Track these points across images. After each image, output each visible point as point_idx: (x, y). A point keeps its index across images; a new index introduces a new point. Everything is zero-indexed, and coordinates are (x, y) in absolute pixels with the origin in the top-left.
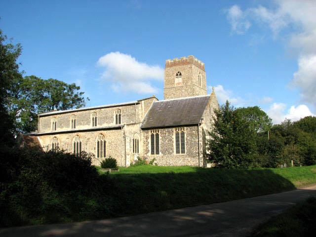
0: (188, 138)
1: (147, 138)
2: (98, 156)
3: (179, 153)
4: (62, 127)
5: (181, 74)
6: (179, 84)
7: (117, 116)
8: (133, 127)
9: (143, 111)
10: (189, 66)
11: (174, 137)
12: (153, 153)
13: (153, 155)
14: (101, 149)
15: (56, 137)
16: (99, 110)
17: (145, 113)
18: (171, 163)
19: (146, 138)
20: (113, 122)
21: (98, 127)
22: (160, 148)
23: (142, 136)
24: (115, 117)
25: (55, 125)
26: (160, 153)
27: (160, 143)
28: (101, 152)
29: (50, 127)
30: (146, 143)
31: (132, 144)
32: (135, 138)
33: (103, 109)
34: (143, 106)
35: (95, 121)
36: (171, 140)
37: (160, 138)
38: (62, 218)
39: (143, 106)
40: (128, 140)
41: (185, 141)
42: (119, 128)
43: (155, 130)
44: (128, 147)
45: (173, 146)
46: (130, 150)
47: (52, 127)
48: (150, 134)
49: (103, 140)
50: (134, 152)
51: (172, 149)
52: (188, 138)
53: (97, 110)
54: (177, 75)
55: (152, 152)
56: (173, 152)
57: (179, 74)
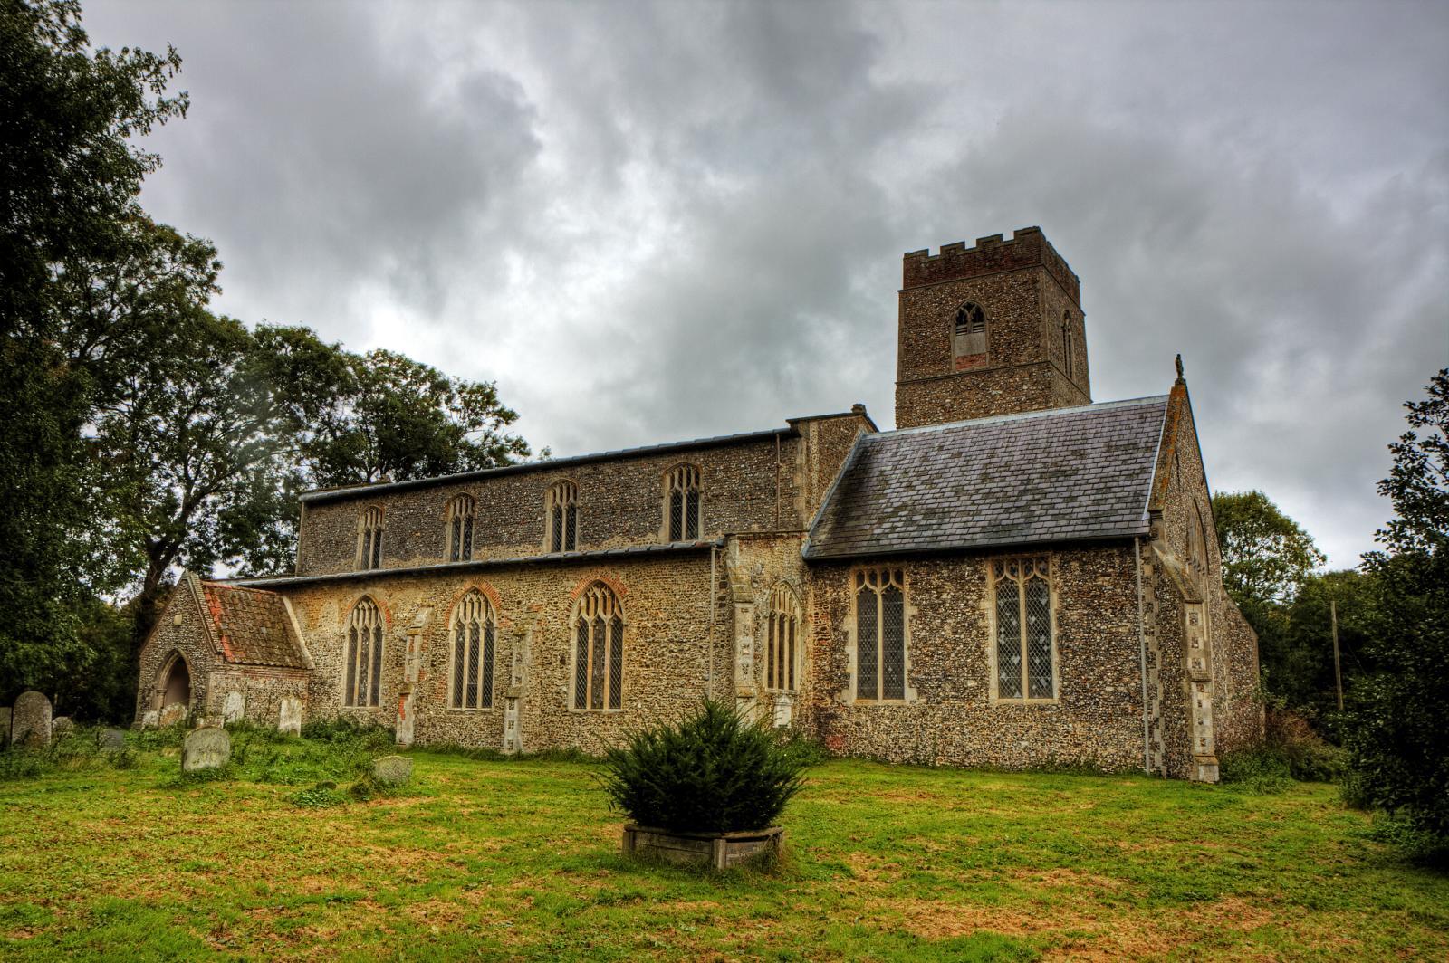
0: (1072, 615)
1: (837, 613)
2: (581, 702)
3: (874, 695)
4: (409, 555)
5: (979, 317)
6: (971, 359)
7: (676, 499)
8: (766, 552)
9: (815, 475)
10: (1023, 277)
11: (988, 606)
12: (867, 691)
13: (870, 703)
14: (599, 664)
15: (366, 599)
16: (586, 470)
17: (822, 485)
18: (970, 747)
19: (834, 614)
20: (655, 531)
21: (580, 550)
22: (908, 665)
23: (811, 600)
24: (666, 506)
25: (377, 544)
26: (910, 693)
27: (908, 640)
28: (598, 681)
29: (349, 554)
30: (832, 636)
31: (766, 641)
32: (779, 611)
33: (608, 469)
34: (814, 449)
35: (567, 522)
36: (971, 624)
37: (910, 611)
38: (1425, 837)
39: (814, 449)
40: (745, 618)
41: (1055, 631)
42: (700, 554)
43: (878, 568)
44: (743, 659)
45: (983, 656)
46: (757, 672)
47: (359, 554)
48: (852, 589)
49: (607, 618)
50: (771, 685)
51: (980, 675)
52: (1072, 615)
53: (579, 471)
54: (961, 319)
55: (861, 682)
56: (984, 685)
57: (971, 317)
